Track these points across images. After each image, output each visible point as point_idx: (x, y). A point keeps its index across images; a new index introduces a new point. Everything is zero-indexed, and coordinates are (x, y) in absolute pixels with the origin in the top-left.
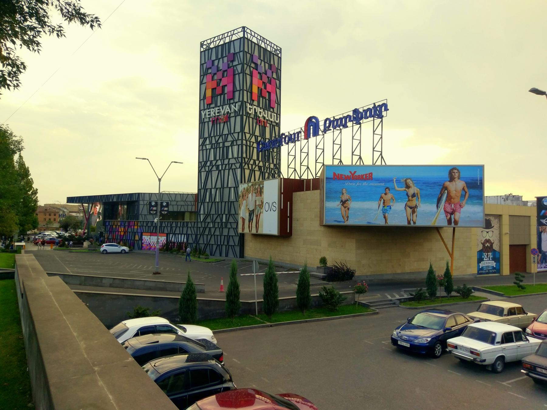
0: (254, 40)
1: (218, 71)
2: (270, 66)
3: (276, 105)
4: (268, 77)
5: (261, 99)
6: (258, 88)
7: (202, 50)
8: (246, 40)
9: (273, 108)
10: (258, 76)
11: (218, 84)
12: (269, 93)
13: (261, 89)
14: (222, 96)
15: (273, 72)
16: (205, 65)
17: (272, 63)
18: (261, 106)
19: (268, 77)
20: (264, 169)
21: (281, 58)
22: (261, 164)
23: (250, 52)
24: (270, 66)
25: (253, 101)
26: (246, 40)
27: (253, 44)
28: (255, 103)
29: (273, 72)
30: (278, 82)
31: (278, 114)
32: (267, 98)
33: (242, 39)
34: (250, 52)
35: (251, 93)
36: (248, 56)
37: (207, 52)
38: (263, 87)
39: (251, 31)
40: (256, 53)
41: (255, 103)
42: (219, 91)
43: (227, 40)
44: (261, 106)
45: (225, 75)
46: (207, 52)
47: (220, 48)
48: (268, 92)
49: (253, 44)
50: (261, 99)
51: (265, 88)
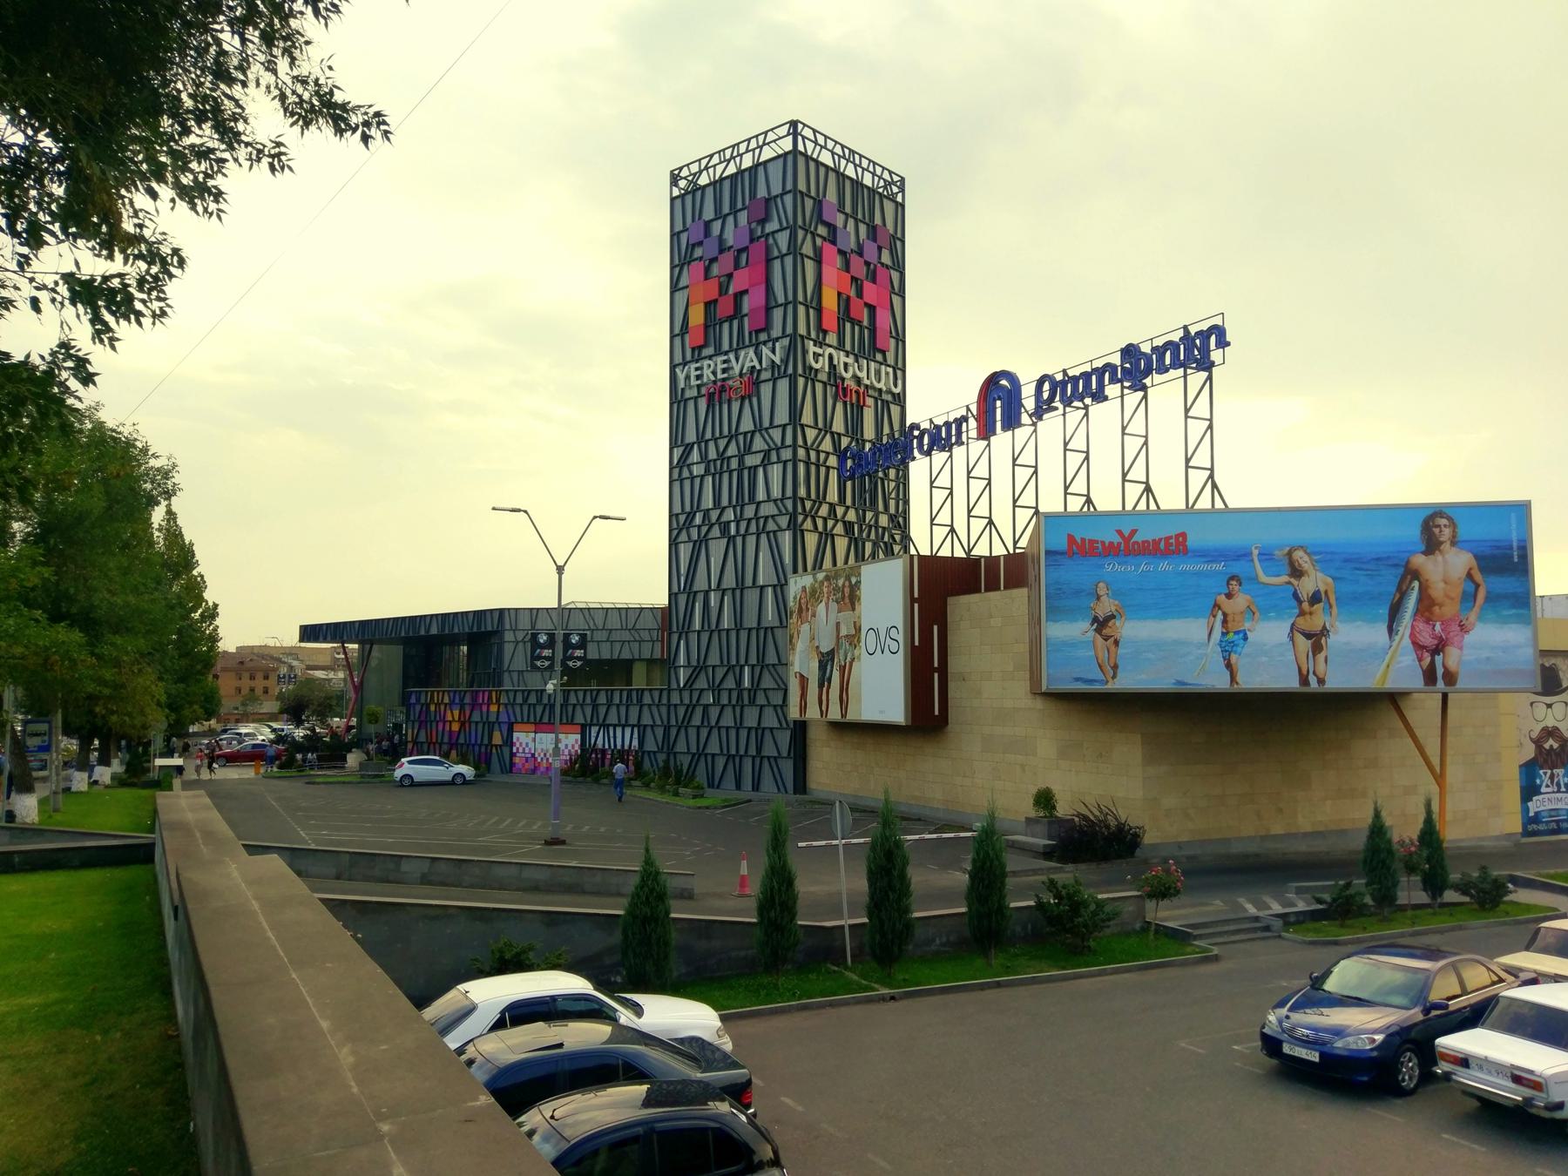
0: (826, 158)
2: (873, 231)
3: (892, 341)
4: (867, 264)
5: (848, 325)
6: (839, 294)
7: (676, 192)
8: (801, 161)
9: (883, 353)
10: (839, 261)
11: (723, 290)
12: (872, 309)
13: (849, 298)
14: (735, 323)
15: (880, 249)
16: (684, 237)
17: (878, 221)
18: (848, 347)
19: (867, 264)
20: (861, 531)
21: (903, 206)
22: (851, 516)
23: (813, 194)
24: (873, 231)
25: (825, 332)
26: (801, 161)
28: (832, 338)
29: (880, 249)
30: (895, 275)
31: (900, 369)
32: (865, 323)
33: (790, 158)
34: (813, 194)
35: (819, 310)
36: (809, 203)
37: (689, 198)
38: (853, 293)
39: (815, 131)
40: (831, 196)
41: (832, 338)
42: (725, 307)
43: (747, 162)
44: (848, 347)
45: (743, 262)
46: (689, 198)
47: (727, 184)
48: (866, 304)
50: (848, 325)
51: (860, 294)
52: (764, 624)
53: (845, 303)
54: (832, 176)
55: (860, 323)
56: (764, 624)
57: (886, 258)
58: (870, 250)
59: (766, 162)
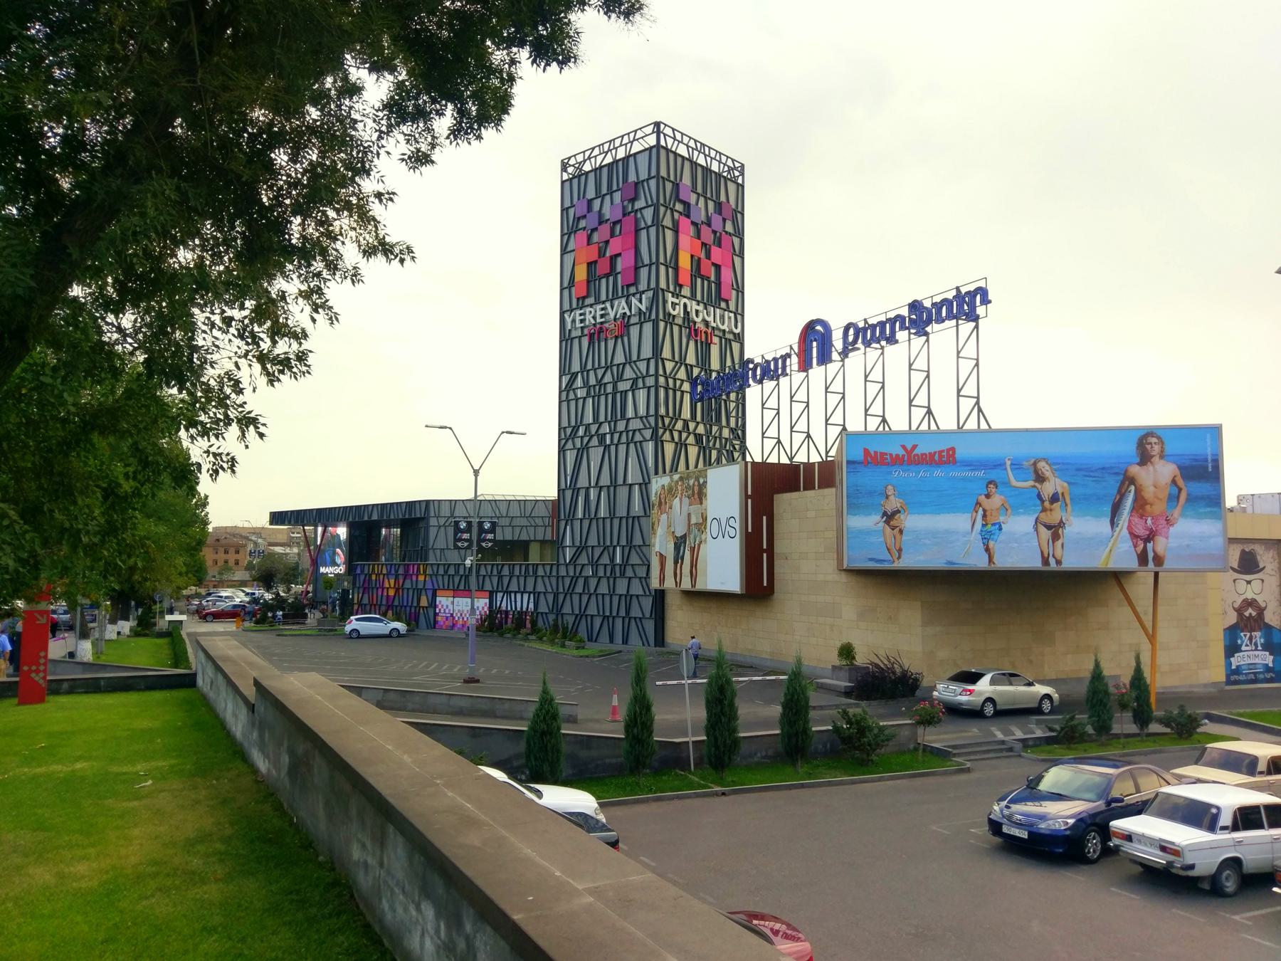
0: (682, 151)
1: (600, 223)
2: (719, 207)
3: (734, 292)
4: (715, 232)
5: (699, 280)
7: (565, 177)
8: (663, 152)
9: (727, 301)
10: (692, 230)
11: (601, 253)
12: (718, 267)
15: (724, 220)
16: (571, 211)
17: (723, 198)
18: (699, 298)
19: (715, 232)
20: (708, 441)
21: (743, 186)
22: (701, 429)
23: (672, 178)
24: (719, 207)
26: (663, 152)
27: (679, 160)
28: (686, 291)
29: (724, 220)
31: (739, 314)
32: (713, 278)
33: (654, 151)
34: (672, 178)
35: (676, 269)
36: (669, 186)
37: (575, 181)
38: (703, 256)
40: (687, 180)
41: (686, 291)
42: (603, 267)
43: (621, 154)
44: (699, 298)
47: (605, 171)
49: (679, 160)
50: (699, 280)
51: (708, 256)
52: (632, 514)
53: (696, 263)
54: (687, 164)
55: (708, 278)
56: (632, 514)
57: (729, 227)
58: (717, 222)
59: (635, 154)
